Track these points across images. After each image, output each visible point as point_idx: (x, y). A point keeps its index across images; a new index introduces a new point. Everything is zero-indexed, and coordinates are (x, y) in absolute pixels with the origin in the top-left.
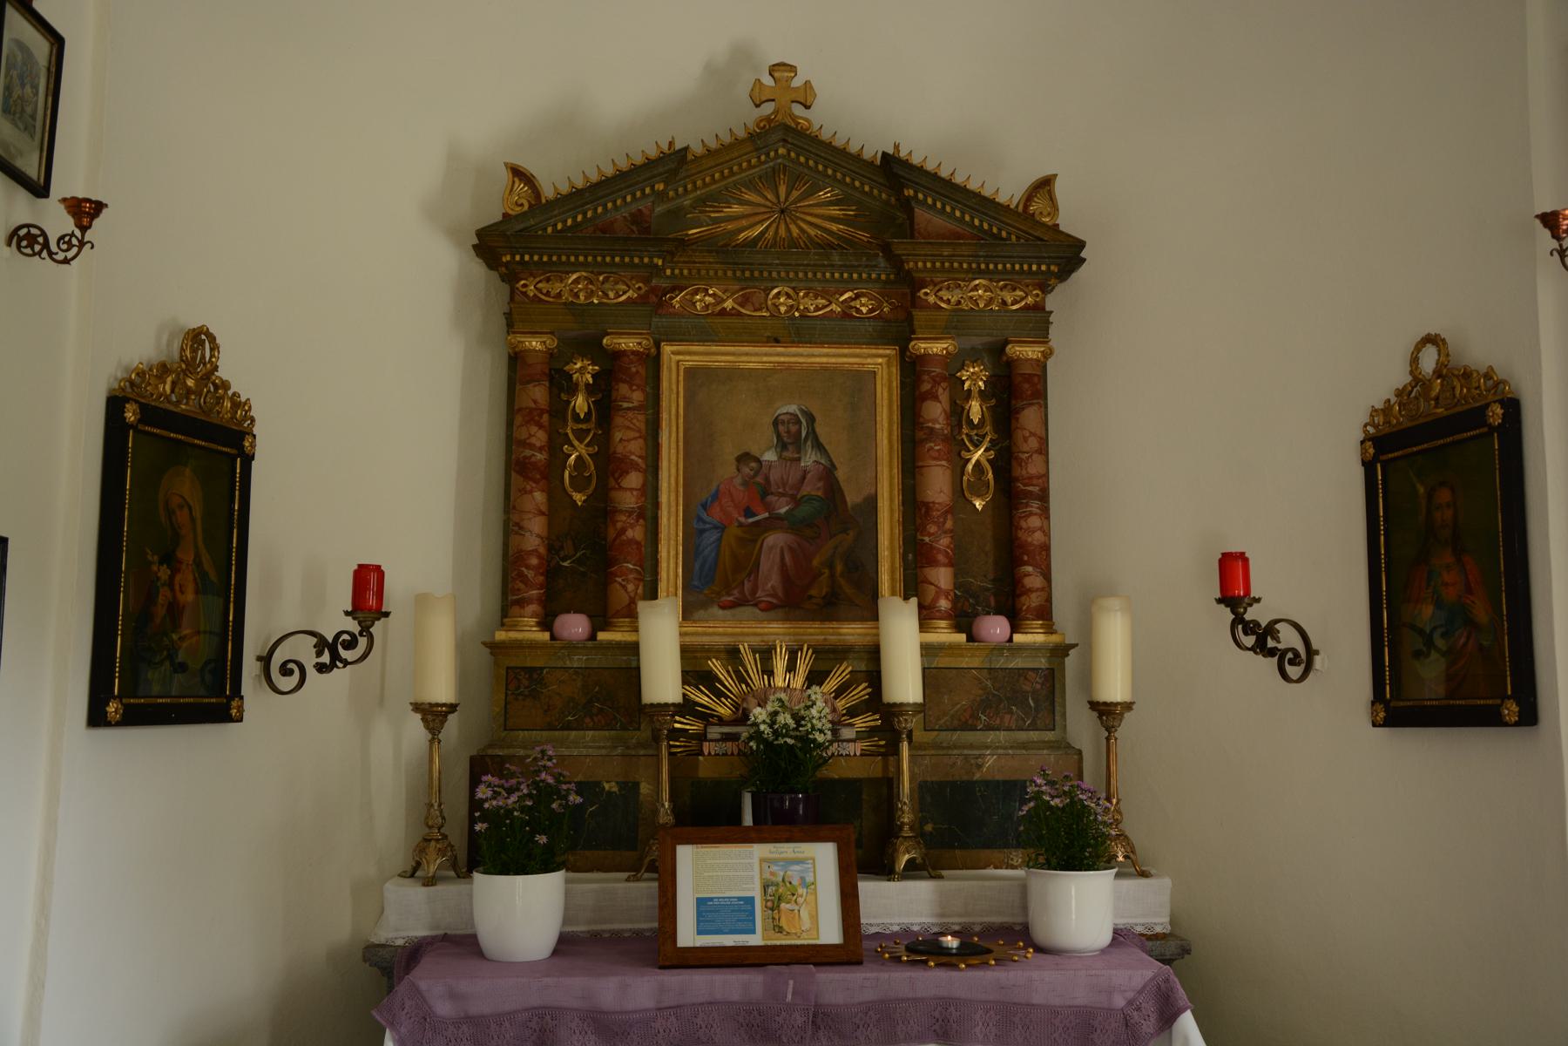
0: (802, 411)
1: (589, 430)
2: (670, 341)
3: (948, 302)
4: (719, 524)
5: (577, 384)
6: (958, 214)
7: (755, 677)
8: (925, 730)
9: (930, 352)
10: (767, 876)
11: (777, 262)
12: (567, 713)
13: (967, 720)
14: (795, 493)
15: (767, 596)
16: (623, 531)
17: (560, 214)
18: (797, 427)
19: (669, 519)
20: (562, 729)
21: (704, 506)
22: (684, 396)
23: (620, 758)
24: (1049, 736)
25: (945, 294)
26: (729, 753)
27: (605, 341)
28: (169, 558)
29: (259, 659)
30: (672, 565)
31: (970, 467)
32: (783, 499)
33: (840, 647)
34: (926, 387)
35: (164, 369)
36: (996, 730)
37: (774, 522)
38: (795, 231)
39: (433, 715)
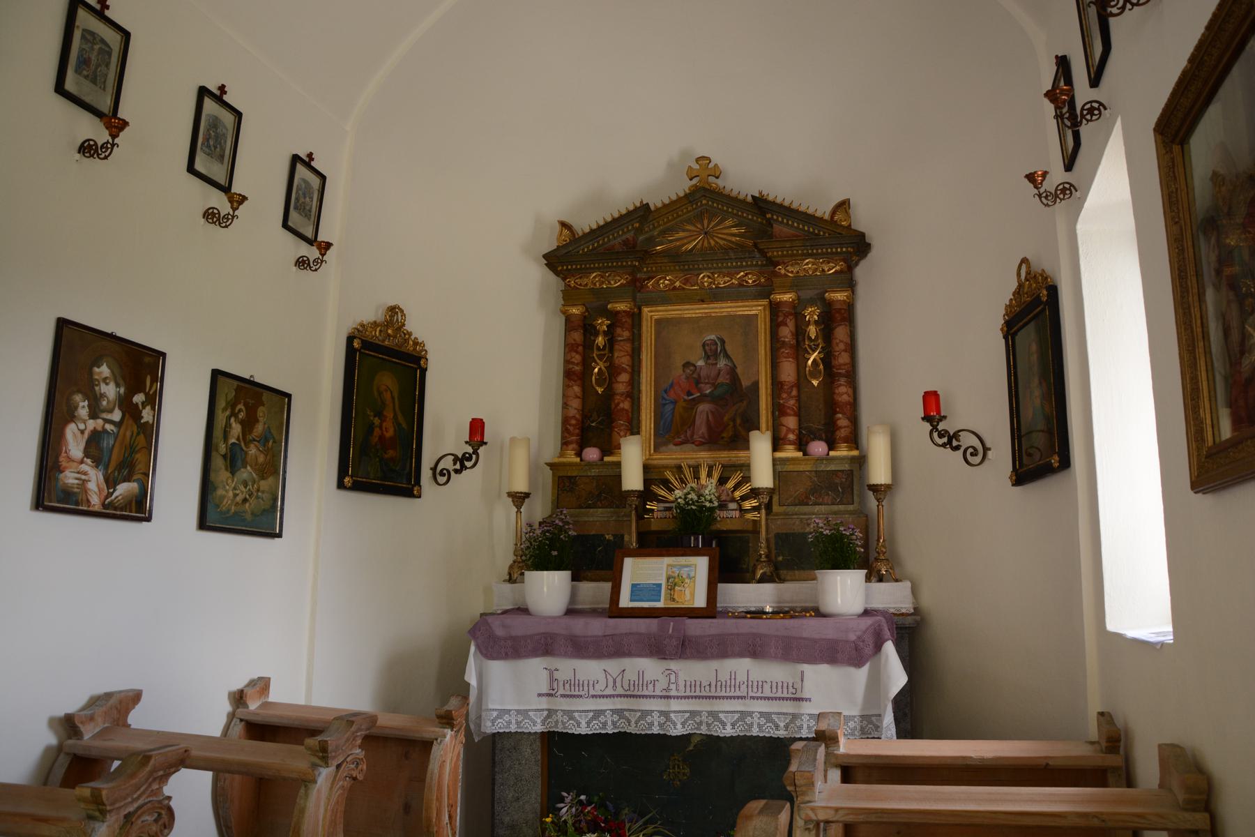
0: (718, 338)
1: (605, 354)
2: (647, 305)
3: (792, 272)
5: (599, 331)
6: (796, 224)
8: (780, 505)
10: (670, 573)
11: (701, 259)
13: (803, 500)
15: (700, 437)
16: (618, 404)
17: (585, 244)
18: (715, 346)
20: (586, 508)
21: (666, 391)
24: (851, 507)
25: (789, 268)
28: (379, 414)
29: (431, 469)
31: (810, 362)
32: (708, 386)
34: (780, 319)
35: (375, 324)
37: (703, 398)
38: (713, 243)
39: (519, 499)
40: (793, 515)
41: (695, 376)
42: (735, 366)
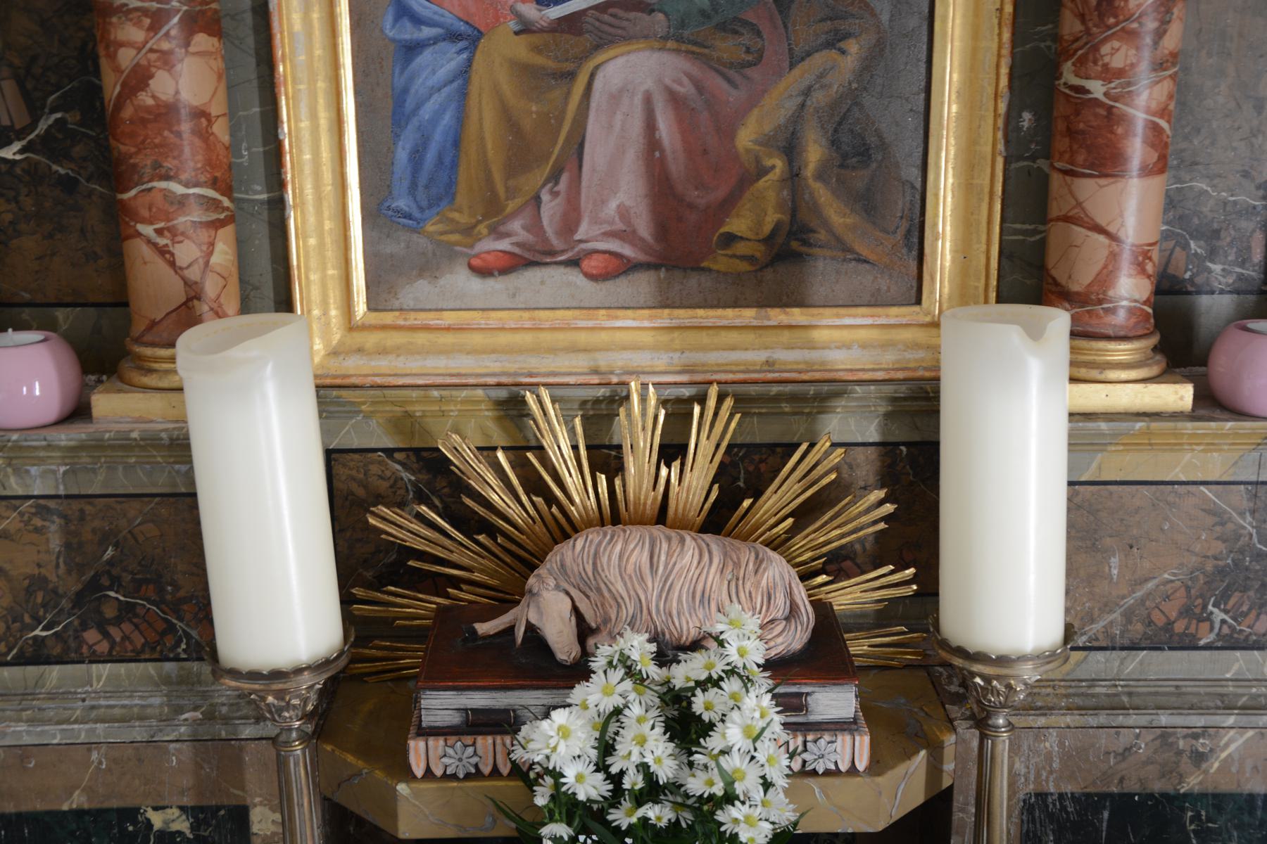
4: (462, 27)
7: (572, 481)
12: (27, 619)
13: (1170, 624)
20: (21, 661)
23: (184, 746)
26: (486, 770)
36: (1252, 648)
40: (1115, 706)
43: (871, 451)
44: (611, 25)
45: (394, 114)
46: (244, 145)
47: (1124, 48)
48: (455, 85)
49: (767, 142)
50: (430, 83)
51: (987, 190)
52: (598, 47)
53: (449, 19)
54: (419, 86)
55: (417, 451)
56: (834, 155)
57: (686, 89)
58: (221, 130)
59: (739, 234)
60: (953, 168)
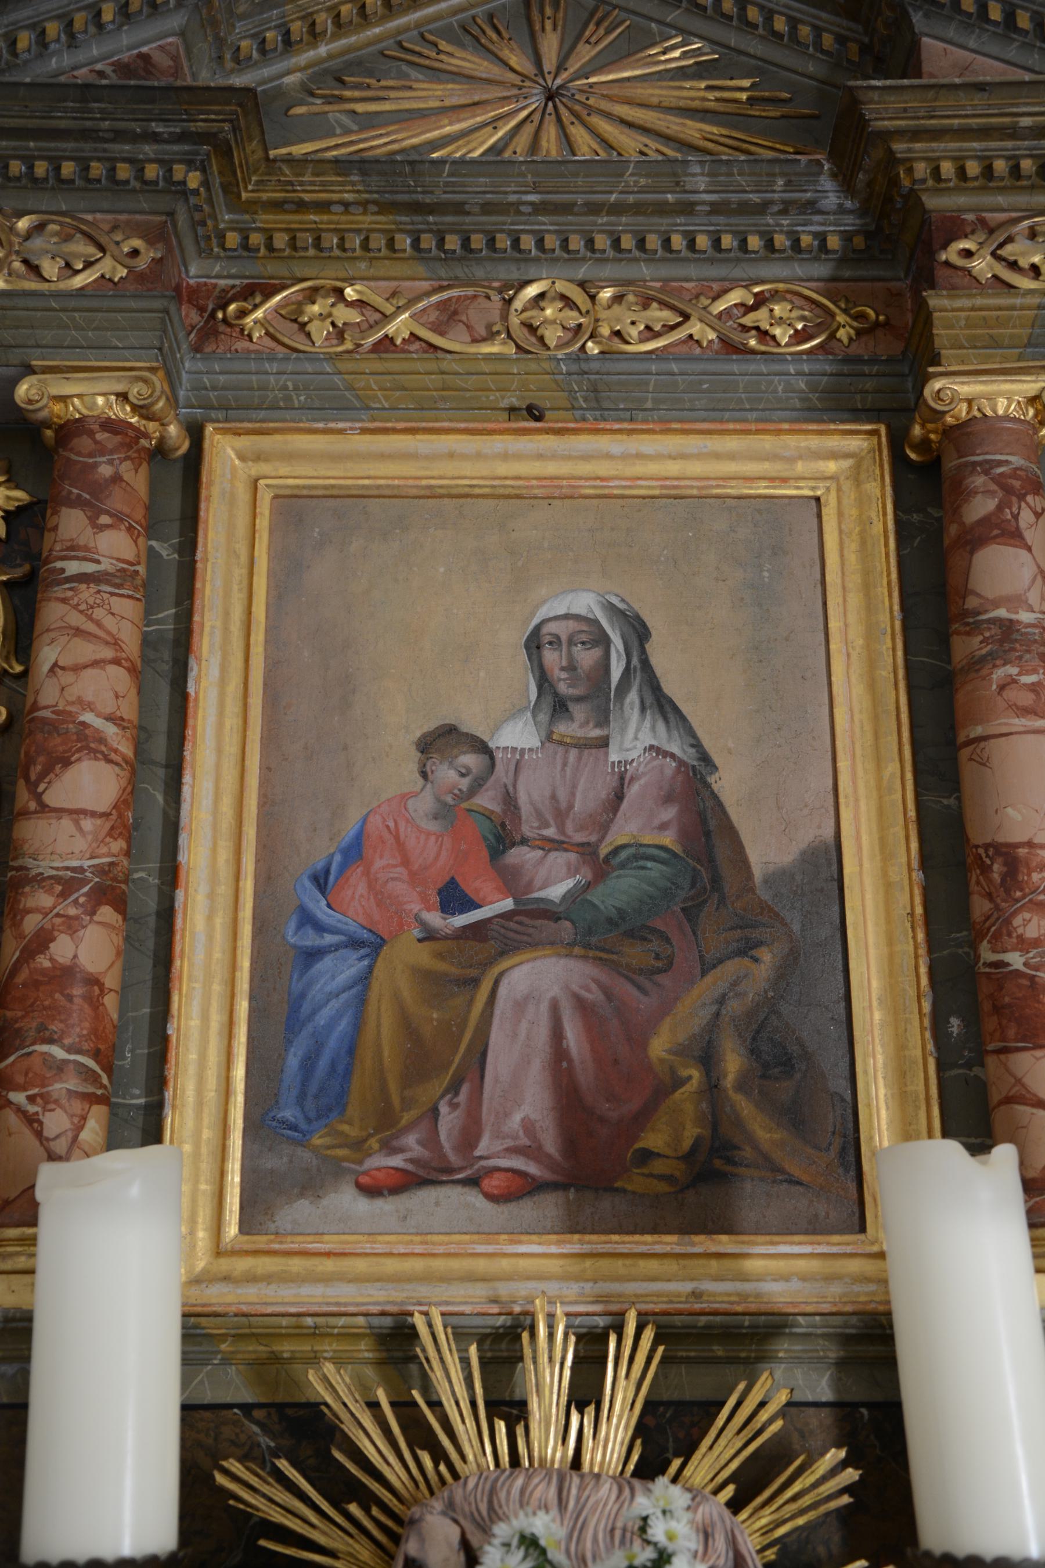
0: (611, 609)
4: (365, 935)
9: (989, 413)
14: (593, 839)
16: (43, 940)
18: (597, 653)
19: (210, 918)
21: (321, 881)
22: (271, 574)
27: (23, 390)
30: (214, 1057)
32: (559, 859)
33: (747, 1321)
41: (487, 800)
42: (705, 758)
43: (825, 1412)
44: (516, 932)
45: (288, 1019)
46: (129, 1046)
47: (1035, 919)
48: (354, 991)
49: (681, 1051)
50: (328, 989)
51: (922, 1096)
52: (502, 954)
53: (352, 927)
54: (316, 993)
55: (280, 1407)
56: (754, 1064)
57: (594, 995)
58: (110, 1002)
59: (656, 1150)
60: (884, 1078)
